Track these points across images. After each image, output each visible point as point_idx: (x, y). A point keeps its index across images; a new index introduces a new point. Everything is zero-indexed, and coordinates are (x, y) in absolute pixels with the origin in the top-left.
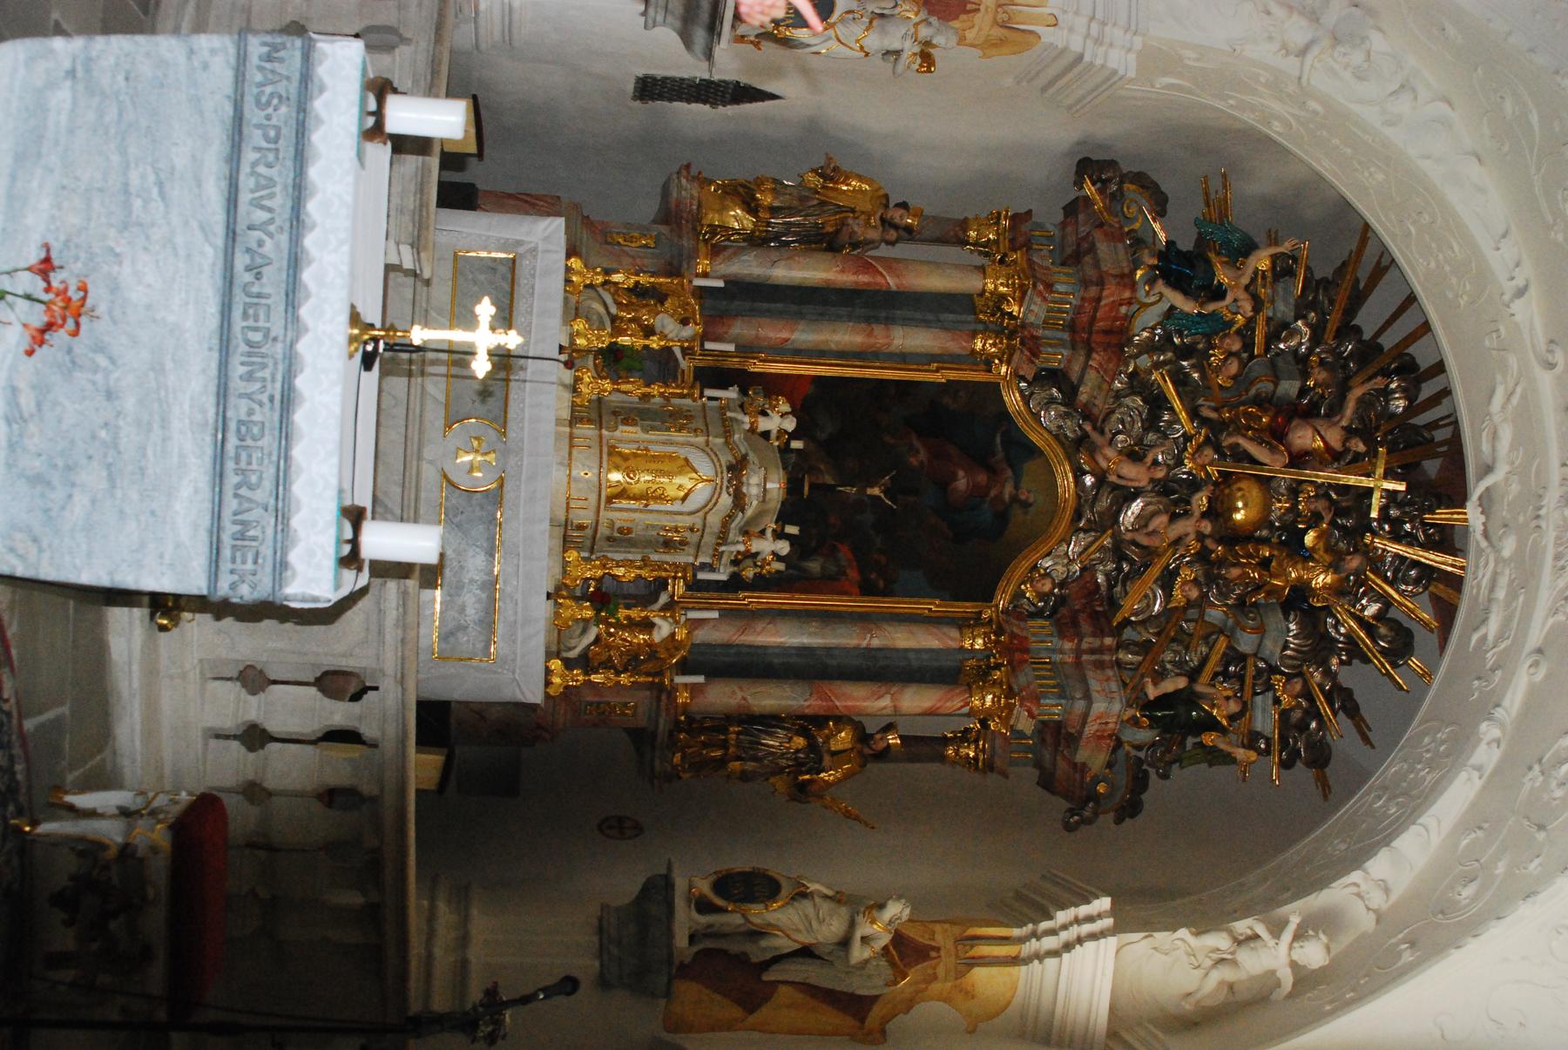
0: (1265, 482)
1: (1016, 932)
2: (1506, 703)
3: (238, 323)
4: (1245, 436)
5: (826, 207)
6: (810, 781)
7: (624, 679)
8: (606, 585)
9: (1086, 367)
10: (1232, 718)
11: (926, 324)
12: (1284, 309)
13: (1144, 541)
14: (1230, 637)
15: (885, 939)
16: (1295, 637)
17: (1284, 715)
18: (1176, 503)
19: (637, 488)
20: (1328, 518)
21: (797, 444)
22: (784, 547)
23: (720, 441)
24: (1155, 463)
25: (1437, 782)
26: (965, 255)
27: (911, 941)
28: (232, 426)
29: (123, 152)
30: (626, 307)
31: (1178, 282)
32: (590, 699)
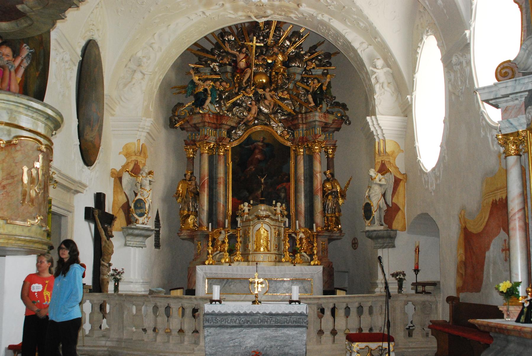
0: (255, 74)
1: (377, 140)
2: (312, 13)
3: (257, 324)
4: (243, 80)
5: (186, 194)
6: (340, 193)
7: (315, 245)
8: (291, 249)
9: (226, 125)
10: (319, 82)
11: (217, 168)
12: (208, 70)
13: (272, 106)
14: (297, 81)
15: (379, 175)
16: (296, 64)
17: (317, 66)
18: (261, 98)
19: (265, 244)
20: (264, 57)
21: (252, 202)
22: (279, 204)
23: (251, 222)
24: (251, 104)
25: (334, 30)
26: (197, 158)
27: (380, 168)
28: (276, 324)
29: (227, 347)
30: (217, 248)
31: (203, 102)
32: (321, 254)
